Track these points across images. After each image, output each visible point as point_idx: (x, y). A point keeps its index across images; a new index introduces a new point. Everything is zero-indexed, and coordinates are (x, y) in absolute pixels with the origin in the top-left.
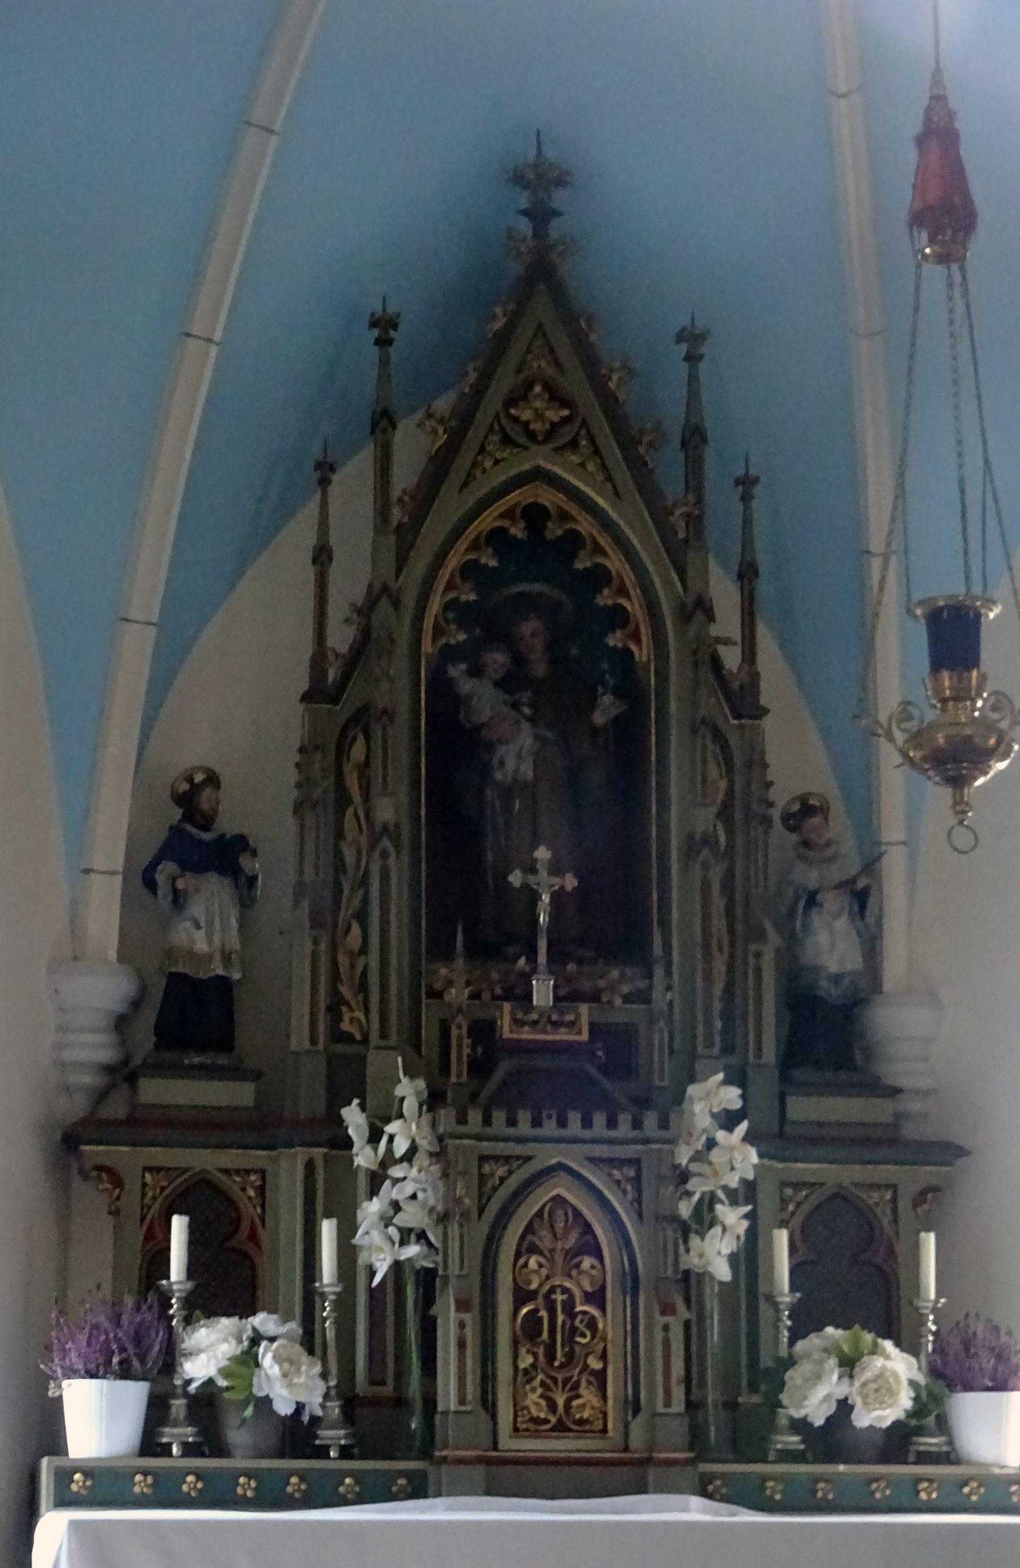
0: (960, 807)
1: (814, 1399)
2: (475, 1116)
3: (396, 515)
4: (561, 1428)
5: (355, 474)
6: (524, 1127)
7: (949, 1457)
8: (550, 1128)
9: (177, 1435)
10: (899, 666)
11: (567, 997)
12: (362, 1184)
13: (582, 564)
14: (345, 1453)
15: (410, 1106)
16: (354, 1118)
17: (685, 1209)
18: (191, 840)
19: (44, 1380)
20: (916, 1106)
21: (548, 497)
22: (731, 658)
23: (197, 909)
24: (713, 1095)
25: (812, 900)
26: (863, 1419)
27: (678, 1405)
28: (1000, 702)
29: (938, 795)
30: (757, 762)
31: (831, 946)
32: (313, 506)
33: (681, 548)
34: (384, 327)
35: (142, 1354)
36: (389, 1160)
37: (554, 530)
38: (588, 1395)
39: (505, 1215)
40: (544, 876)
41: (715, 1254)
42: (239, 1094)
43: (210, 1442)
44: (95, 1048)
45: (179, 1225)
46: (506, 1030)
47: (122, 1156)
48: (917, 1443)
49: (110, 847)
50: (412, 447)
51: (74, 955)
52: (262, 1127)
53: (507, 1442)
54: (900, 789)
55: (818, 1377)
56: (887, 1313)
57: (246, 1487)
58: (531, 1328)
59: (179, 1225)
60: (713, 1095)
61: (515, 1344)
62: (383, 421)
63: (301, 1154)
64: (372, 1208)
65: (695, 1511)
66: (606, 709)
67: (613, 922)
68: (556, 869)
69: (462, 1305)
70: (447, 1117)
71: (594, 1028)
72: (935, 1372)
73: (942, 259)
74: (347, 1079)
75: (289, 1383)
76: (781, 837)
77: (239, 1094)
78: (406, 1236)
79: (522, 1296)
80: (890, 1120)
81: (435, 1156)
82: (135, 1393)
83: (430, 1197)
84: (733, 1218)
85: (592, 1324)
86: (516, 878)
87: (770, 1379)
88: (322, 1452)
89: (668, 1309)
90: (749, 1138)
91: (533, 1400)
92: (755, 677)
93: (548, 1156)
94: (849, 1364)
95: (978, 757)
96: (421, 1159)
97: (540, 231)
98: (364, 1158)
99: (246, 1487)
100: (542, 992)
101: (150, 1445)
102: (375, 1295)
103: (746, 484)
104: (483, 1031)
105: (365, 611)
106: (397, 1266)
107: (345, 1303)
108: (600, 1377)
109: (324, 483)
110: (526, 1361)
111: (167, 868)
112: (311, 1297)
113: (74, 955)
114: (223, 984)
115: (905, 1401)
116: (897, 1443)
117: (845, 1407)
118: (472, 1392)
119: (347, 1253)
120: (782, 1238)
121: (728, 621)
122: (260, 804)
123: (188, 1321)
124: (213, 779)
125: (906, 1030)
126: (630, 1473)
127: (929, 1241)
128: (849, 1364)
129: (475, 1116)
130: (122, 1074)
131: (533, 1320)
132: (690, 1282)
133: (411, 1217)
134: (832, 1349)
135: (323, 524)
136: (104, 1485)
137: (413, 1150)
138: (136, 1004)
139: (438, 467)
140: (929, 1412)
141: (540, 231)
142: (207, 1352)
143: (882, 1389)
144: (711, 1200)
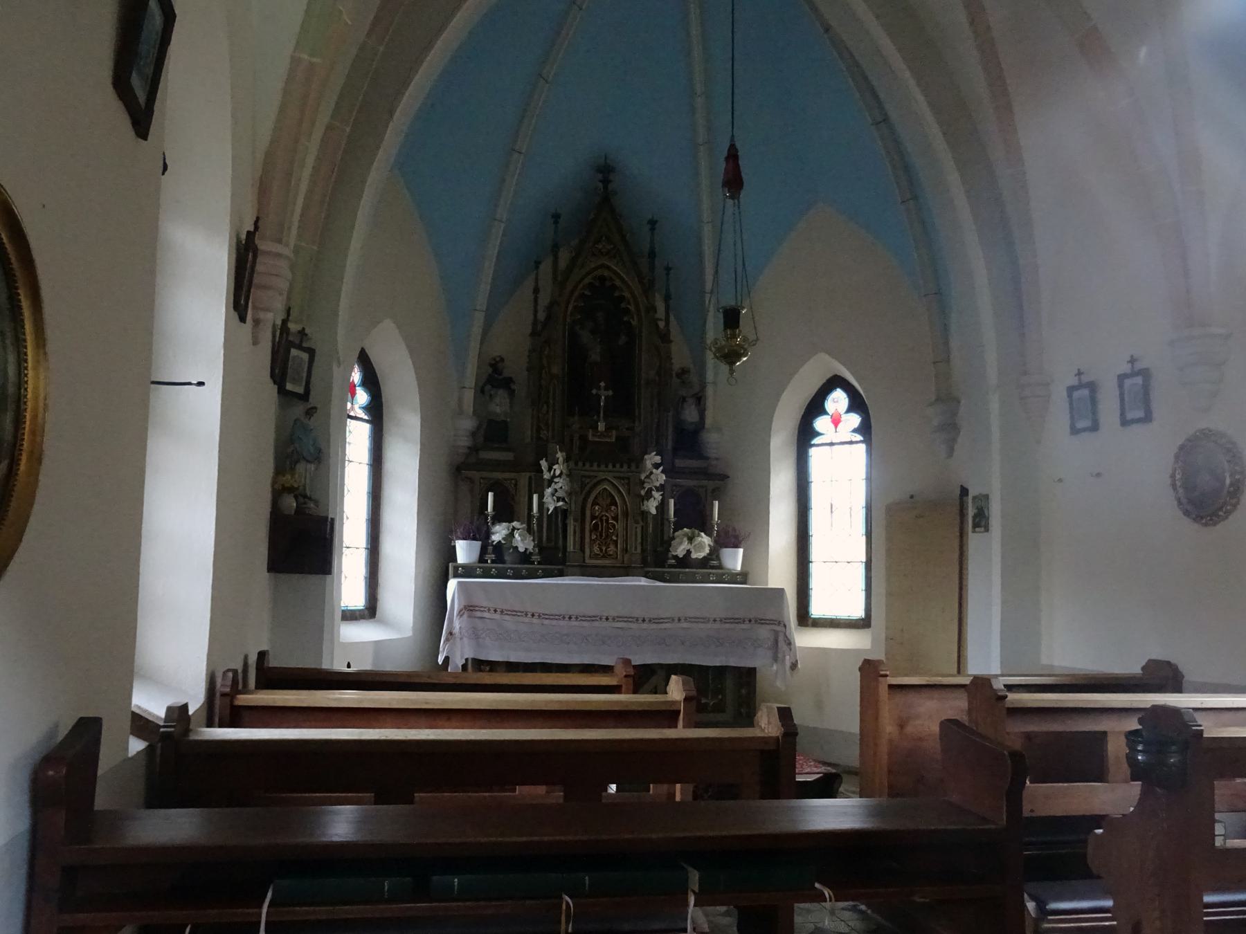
0: (732, 371)
1: (680, 551)
2: (580, 464)
3: (559, 278)
4: (604, 557)
5: (546, 266)
6: (595, 467)
7: (720, 567)
8: (603, 467)
9: (490, 557)
10: (713, 328)
11: (608, 429)
12: (546, 483)
13: (623, 305)
14: (539, 563)
15: (561, 460)
16: (544, 464)
17: (643, 493)
18: (494, 378)
19: (451, 540)
20: (714, 462)
21: (606, 273)
22: (662, 324)
23: (497, 400)
24: (653, 458)
25: (684, 399)
26: (694, 556)
27: (639, 550)
28: (745, 339)
29: (724, 368)
30: (669, 358)
31: (690, 414)
32: (533, 276)
33: (648, 288)
34: (556, 217)
35: (479, 533)
36: (554, 476)
37: (608, 284)
38: (612, 547)
39: (589, 493)
40: (603, 394)
41: (652, 506)
42: (509, 456)
43: (499, 559)
44: (464, 442)
45: (490, 495)
46: (590, 438)
47: (475, 475)
48: (711, 564)
49: (470, 380)
50: (564, 258)
51: (460, 412)
52: (515, 466)
53: (587, 561)
54: (714, 369)
55: (681, 543)
56: (703, 525)
57: (510, 572)
58: (596, 527)
59: (490, 495)
60: (653, 458)
61: (591, 532)
62: (555, 248)
63: (528, 474)
64: (549, 490)
65: (643, 582)
66: (623, 339)
67: (623, 406)
68: (606, 389)
69: (575, 520)
70: (572, 464)
71: (617, 438)
72: (716, 542)
73: (732, 197)
74: (543, 452)
75: (522, 542)
76: (675, 380)
77: (509, 456)
78: (559, 499)
79: (593, 517)
80: (1095, 871)
81: (568, 476)
82: (478, 544)
83: (566, 488)
84: (657, 495)
85: (614, 526)
86: (594, 392)
87: (667, 543)
88: (533, 563)
89: (637, 522)
90: (663, 472)
91: (596, 549)
92: (669, 331)
93: (602, 476)
94: (691, 539)
95: (739, 357)
96: (564, 476)
97: (606, 188)
98: (546, 476)
99: (510, 572)
100: (601, 426)
101: (482, 559)
102: (549, 517)
103: (668, 269)
104: (583, 438)
105: (550, 308)
106: (556, 508)
107: (540, 519)
108: (616, 543)
109: (537, 268)
110: (594, 537)
111: (488, 387)
112: (530, 516)
113: (460, 412)
114: (505, 422)
115: (707, 550)
116: (704, 563)
117: (689, 552)
118: (578, 546)
119: (541, 504)
120: (672, 502)
121: (661, 312)
122: (517, 368)
123: (493, 524)
124: (502, 360)
125: (713, 440)
126: (626, 571)
127: (716, 503)
128: (691, 539)
129: (580, 464)
130: (474, 449)
131: (596, 525)
132: (644, 514)
133: (560, 494)
134: (686, 535)
135: (537, 280)
136: (468, 571)
137: (560, 476)
138: (479, 428)
139: (573, 261)
140: (714, 553)
141: (606, 188)
142: (499, 533)
143: (700, 547)
144: (650, 490)
